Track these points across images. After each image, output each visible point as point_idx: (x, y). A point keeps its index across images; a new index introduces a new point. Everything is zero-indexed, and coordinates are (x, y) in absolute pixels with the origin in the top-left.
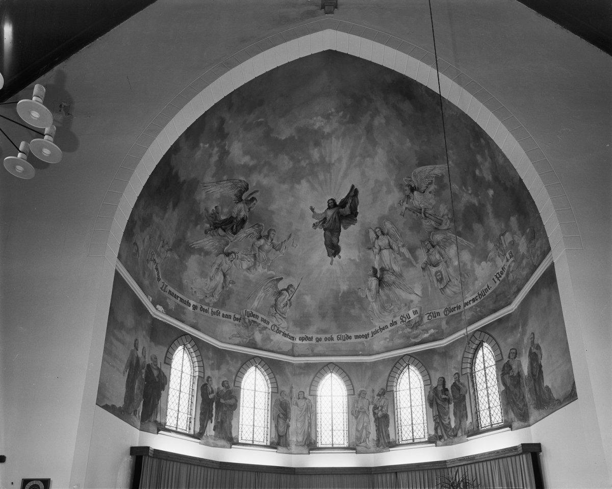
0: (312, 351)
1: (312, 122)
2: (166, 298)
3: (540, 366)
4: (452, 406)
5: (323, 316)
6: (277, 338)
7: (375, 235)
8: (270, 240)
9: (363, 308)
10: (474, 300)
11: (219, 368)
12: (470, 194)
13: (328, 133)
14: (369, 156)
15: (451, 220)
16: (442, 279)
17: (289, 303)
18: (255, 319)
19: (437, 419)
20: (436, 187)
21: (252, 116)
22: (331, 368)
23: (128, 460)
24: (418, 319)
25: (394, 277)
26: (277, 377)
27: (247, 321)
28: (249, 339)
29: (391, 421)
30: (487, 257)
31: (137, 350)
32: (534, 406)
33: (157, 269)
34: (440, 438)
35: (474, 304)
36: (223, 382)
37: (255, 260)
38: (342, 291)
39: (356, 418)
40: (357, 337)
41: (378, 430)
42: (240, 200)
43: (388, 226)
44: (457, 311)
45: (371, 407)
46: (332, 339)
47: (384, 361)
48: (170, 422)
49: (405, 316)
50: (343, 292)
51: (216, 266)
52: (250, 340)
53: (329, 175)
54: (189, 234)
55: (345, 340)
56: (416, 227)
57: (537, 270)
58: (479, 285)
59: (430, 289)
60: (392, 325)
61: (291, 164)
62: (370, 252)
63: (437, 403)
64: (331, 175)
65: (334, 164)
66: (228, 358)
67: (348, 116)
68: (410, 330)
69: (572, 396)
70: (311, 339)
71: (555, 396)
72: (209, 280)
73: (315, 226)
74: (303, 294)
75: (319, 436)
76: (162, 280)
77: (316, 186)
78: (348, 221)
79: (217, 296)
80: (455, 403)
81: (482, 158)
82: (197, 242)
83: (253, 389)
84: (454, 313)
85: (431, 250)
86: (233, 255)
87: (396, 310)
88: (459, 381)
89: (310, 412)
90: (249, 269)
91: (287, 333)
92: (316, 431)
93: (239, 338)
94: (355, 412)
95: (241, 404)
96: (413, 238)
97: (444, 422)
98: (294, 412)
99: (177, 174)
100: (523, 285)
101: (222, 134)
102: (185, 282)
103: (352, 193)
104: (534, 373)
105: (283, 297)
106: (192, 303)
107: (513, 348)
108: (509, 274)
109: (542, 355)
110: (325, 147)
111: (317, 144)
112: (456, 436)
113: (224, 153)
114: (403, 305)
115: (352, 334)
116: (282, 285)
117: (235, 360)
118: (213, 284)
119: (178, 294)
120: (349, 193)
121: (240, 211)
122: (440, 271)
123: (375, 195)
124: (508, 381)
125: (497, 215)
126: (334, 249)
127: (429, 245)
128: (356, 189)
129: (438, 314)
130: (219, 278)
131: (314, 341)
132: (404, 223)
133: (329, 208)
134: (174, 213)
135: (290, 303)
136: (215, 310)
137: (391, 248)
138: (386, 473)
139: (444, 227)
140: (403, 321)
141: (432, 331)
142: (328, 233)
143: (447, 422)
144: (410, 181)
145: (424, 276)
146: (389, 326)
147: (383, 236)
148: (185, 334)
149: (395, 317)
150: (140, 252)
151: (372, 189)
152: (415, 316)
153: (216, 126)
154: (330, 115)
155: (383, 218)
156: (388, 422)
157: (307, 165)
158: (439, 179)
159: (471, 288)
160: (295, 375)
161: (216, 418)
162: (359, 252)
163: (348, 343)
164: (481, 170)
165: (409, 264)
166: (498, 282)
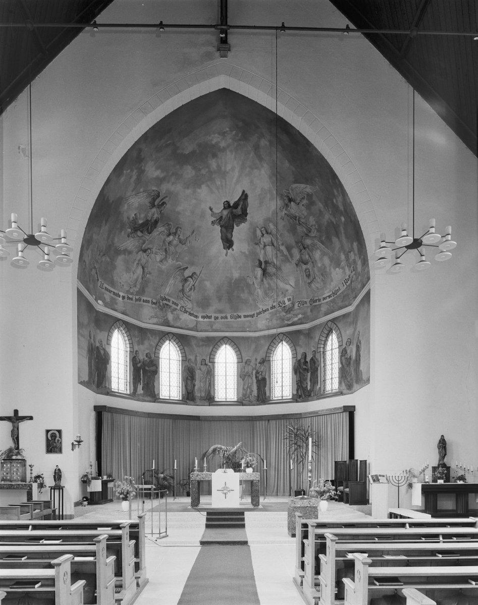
0: (212, 327)
4: (309, 374)
5: (220, 299)
6: (185, 317)
8: (177, 236)
9: (251, 293)
10: (329, 296)
11: (143, 344)
14: (257, 168)
15: (318, 230)
16: (309, 275)
17: (193, 288)
21: (163, 141)
22: (226, 341)
23: (93, 414)
25: (275, 270)
27: (161, 304)
29: (268, 383)
34: (300, 396)
36: (147, 354)
37: (166, 253)
39: (243, 380)
40: (245, 316)
41: (259, 389)
45: (254, 372)
46: (226, 318)
47: (264, 337)
48: (114, 386)
50: (236, 279)
51: (137, 262)
53: (224, 181)
54: (116, 240)
56: (293, 230)
60: (272, 308)
61: (194, 173)
63: (299, 371)
64: (226, 181)
66: (149, 335)
67: (240, 135)
68: (285, 314)
70: (210, 317)
73: (213, 223)
74: (204, 280)
75: (217, 393)
76: (100, 280)
78: (239, 220)
79: (138, 286)
80: (311, 372)
86: (149, 250)
89: (210, 374)
90: (161, 261)
91: (192, 312)
92: (214, 389)
94: (242, 376)
95: (160, 370)
96: (291, 240)
98: (198, 374)
102: (115, 278)
103: (243, 197)
105: (188, 283)
106: (121, 294)
111: (215, 156)
112: (310, 396)
114: (280, 293)
115: (242, 314)
116: (187, 273)
119: (112, 289)
120: (240, 197)
121: (153, 215)
122: (308, 269)
124: (344, 361)
125: (347, 237)
126: (228, 243)
128: (246, 194)
129: (306, 302)
130: (139, 271)
131: (213, 319)
133: (225, 208)
135: (194, 288)
136: (137, 297)
137: (273, 245)
138: (262, 420)
139: (313, 234)
140: (280, 306)
141: (300, 316)
142: (224, 230)
143: (305, 386)
148: (118, 320)
149: (274, 302)
154: (224, 133)
155: (268, 220)
156: (266, 384)
157: (206, 173)
158: (309, 196)
161: (144, 382)
164: (337, 201)
165: (286, 260)
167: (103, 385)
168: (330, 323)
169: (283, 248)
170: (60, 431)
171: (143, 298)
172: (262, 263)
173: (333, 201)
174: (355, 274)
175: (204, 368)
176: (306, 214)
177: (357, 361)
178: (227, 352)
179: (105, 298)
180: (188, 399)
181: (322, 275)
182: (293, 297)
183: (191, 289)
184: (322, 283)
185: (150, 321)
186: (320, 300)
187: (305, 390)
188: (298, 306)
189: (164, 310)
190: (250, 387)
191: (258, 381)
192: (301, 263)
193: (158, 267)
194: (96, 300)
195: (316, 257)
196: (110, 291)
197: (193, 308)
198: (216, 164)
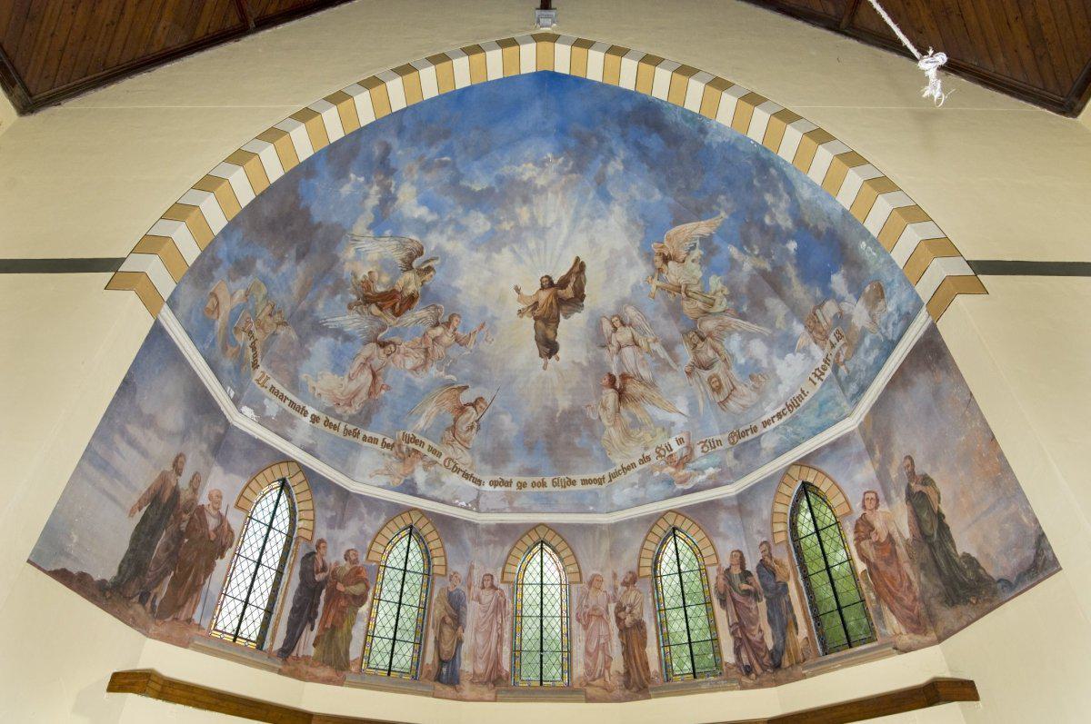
0: (511, 503)
1: (519, 170)
2: (263, 397)
3: (940, 516)
5: (531, 448)
6: (455, 479)
8: (451, 330)
9: (594, 437)
10: (779, 416)
12: (758, 256)
13: (542, 186)
14: (599, 217)
15: (730, 298)
18: (417, 447)
19: (736, 630)
20: (702, 253)
21: (434, 151)
24: (685, 452)
25: (643, 388)
26: (447, 546)
27: (404, 449)
28: (404, 478)
30: (794, 346)
32: (940, 599)
33: (254, 348)
34: (748, 670)
35: (781, 421)
36: (349, 551)
37: (426, 357)
39: (585, 627)
40: (585, 482)
41: (627, 653)
42: (409, 267)
43: (631, 313)
44: (751, 436)
45: (612, 607)
46: (544, 484)
49: (664, 447)
50: (563, 411)
51: (361, 360)
52: (406, 480)
53: (542, 243)
54: (321, 305)
55: (565, 487)
57: (896, 351)
59: (701, 403)
61: (488, 226)
62: (605, 351)
63: (733, 600)
64: (546, 243)
65: (550, 228)
66: (363, 510)
67: (571, 163)
68: (673, 470)
69: (1040, 564)
70: (508, 484)
71: (994, 572)
72: (346, 380)
76: (261, 368)
81: (774, 195)
82: (334, 320)
84: (747, 439)
87: (649, 438)
88: (771, 558)
90: (415, 369)
93: (388, 477)
96: (671, 330)
97: (751, 637)
98: (473, 613)
99: (307, 208)
100: (872, 380)
101: (384, 167)
102: (303, 377)
103: (577, 269)
104: (927, 529)
105: (467, 415)
107: (868, 489)
108: (838, 367)
109: (939, 494)
111: (526, 200)
112: (777, 666)
113: (388, 199)
114: (659, 429)
115: (577, 477)
116: (466, 397)
118: (353, 386)
119: (287, 393)
120: (572, 269)
121: (409, 283)
122: (716, 376)
126: (549, 347)
127: (696, 337)
128: (582, 263)
129: (719, 442)
130: (366, 378)
131: (514, 488)
133: (543, 288)
134: (298, 268)
135: (479, 426)
136: (351, 427)
139: (718, 308)
141: (711, 471)
142: (540, 324)
144: (662, 247)
145: (691, 385)
146: (637, 463)
147: (623, 328)
149: (646, 448)
152: (681, 446)
154: (544, 162)
155: (623, 302)
157: (511, 228)
158: (706, 242)
159: (772, 396)
160: (479, 544)
161: (324, 622)
162: (588, 352)
163: (570, 491)
164: (773, 217)
165: (666, 367)
167: (183, 615)
168: (795, 472)
169: (657, 347)
171: (363, 432)
175: (487, 596)
176: (700, 274)
178: (545, 559)
179: (264, 408)
180: (438, 678)
181: (751, 377)
182: (689, 434)
183: (472, 427)
185: (373, 481)
186: (754, 429)
187: (759, 648)
188: (703, 451)
189: (408, 460)
190: (603, 648)
191: (624, 631)
192: (697, 369)
197: (472, 465)
198: (528, 215)
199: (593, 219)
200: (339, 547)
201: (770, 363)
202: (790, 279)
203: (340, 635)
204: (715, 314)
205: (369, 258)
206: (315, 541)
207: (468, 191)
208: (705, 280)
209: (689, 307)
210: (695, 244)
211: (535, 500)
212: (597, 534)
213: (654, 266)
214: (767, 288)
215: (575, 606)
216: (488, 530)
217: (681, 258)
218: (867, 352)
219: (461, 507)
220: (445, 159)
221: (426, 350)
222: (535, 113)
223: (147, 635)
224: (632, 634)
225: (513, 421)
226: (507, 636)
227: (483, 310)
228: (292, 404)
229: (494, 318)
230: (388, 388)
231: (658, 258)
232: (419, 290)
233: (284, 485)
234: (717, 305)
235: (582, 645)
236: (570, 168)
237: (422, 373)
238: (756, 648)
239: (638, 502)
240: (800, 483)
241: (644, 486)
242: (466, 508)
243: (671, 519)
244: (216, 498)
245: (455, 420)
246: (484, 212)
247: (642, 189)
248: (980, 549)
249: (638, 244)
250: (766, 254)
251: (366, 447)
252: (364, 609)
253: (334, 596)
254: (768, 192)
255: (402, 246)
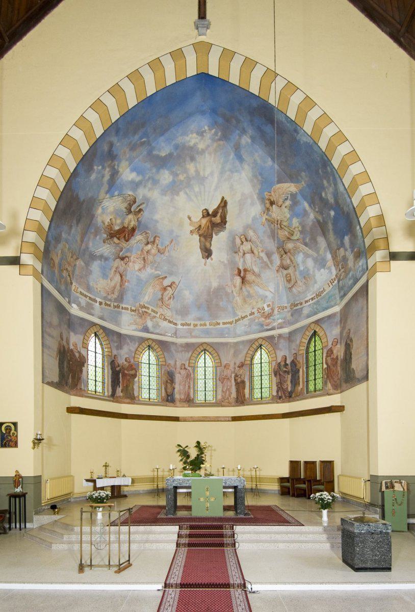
1: (187, 138)
2: (78, 298)
3: (351, 354)
4: (290, 376)
5: (199, 307)
7: (240, 241)
8: (155, 245)
10: (312, 299)
13: (202, 149)
14: (237, 171)
15: (301, 232)
16: (290, 280)
18: (146, 310)
21: (137, 137)
24: (270, 311)
27: (141, 312)
31: (63, 340)
33: (69, 276)
34: (280, 398)
35: (313, 302)
38: (213, 288)
39: (222, 383)
40: (224, 323)
41: (238, 391)
42: (130, 212)
43: (251, 234)
44: (299, 307)
45: (233, 375)
46: (205, 325)
47: (243, 342)
51: (114, 269)
54: (91, 244)
58: (316, 288)
60: (251, 314)
61: (171, 178)
62: (236, 255)
64: (204, 188)
65: (207, 178)
67: (219, 134)
68: (264, 319)
69: (366, 378)
70: (189, 325)
72: (109, 281)
73: (191, 232)
76: (74, 284)
77: (193, 197)
78: (218, 229)
83: (148, 375)
85: (284, 256)
87: (255, 304)
88: (296, 359)
94: (220, 379)
96: (271, 245)
98: (178, 378)
99: (77, 195)
100: (349, 291)
101: (111, 156)
102: (91, 284)
103: (223, 204)
105: (167, 292)
106: (98, 300)
110: (200, 162)
111: (193, 159)
112: (290, 397)
113: (115, 174)
114: (260, 299)
116: (166, 282)
117: (133, 342)
118: (113, 284)
119: (87, 294)
120: (220, 204)
121: (130, 221)
122: (289, 274)
123: (241, 204)
125: (336, 232)
128: (226, 200)
131: (192, 327)
132: (264, 232)
133: (203, 217)
136: (116, 304)
137: (253, 252)
139: (295, 237)
141: (280, 321)
142: (203, 239)
143: (285, 387)
149: (253, 309)
150: (56, 265)
151: (239, 201)
153: (106, 150)
154: (203, 132)
155: (247, 227)
158: (293, 196)
159: (311, 289)
161: (123, 384)
162: (228, 255)
164: (326, 194)
165: (265, 266)
166: (331, 286)
168: (312, 326)
169: (263, 255)
170: (15, 424)
171: (121, 305)
172: (241, 271)
173: (321, 195)
174: (343, 271)
175: (183, 372)
176: (288, 216)
177: (346, 359)
178: (206, 357)
179: (80, 303)
180: (167, 401)
181: (304, 277)
182: (273, 302)
184: (304, 286)
186: (301, 304)
190: (229, 390)
191: (237, 384)
193: (137, 275)
194: (69, 302)
195: (298, 260)
196: (86, 296)
197: (172, 316)
199: (232, 172)
200: (123, 355)
201: (314, 271)
202: (329, 230)
203: (130, 388)
204: (293, 240)
205: (108, 211)
206: (113, 356)
207: (158, 157)
208: (290, 219)
209: (283, 234)
210: (288, 197)
211: (202, 332)
212: (229, 346)
213: (265, 206)
214: (319, 231)
215: (218, 375)
216: (181, 345)
217: (280, 204)
218: (350, 279)
219: (169, 336)
220: (144, 140)
221: (144, 259)
222: (197, 100)
223: (70, 395)
224: (240, 385)
225: (190, 293)
226: (192, 386)
227: (171, 232)
228: (90, 298)
229: (178, 236)
230: (129, 281)
231: (268, 202)
232: (136, 224)
233: (96, 335)
234: (294, 235)
235: (221, 389)
236: (219, 137)
237: (143, 271)
238: (284, 391)
239: (247, 333)
240: (313, 331)
241: (250, 326)
242: (171, 337)
243: (260, 342)
244: (75, 345)
245: (162, 295)
246: (168, 170)
247: (259, 156)
248: (356, 368)
249: (257, 191)
250: (321, 213)
251: (124, 312)
252: (136, 379)
253: (124, 375)
254: (325, 179)
255: (125, 199)
